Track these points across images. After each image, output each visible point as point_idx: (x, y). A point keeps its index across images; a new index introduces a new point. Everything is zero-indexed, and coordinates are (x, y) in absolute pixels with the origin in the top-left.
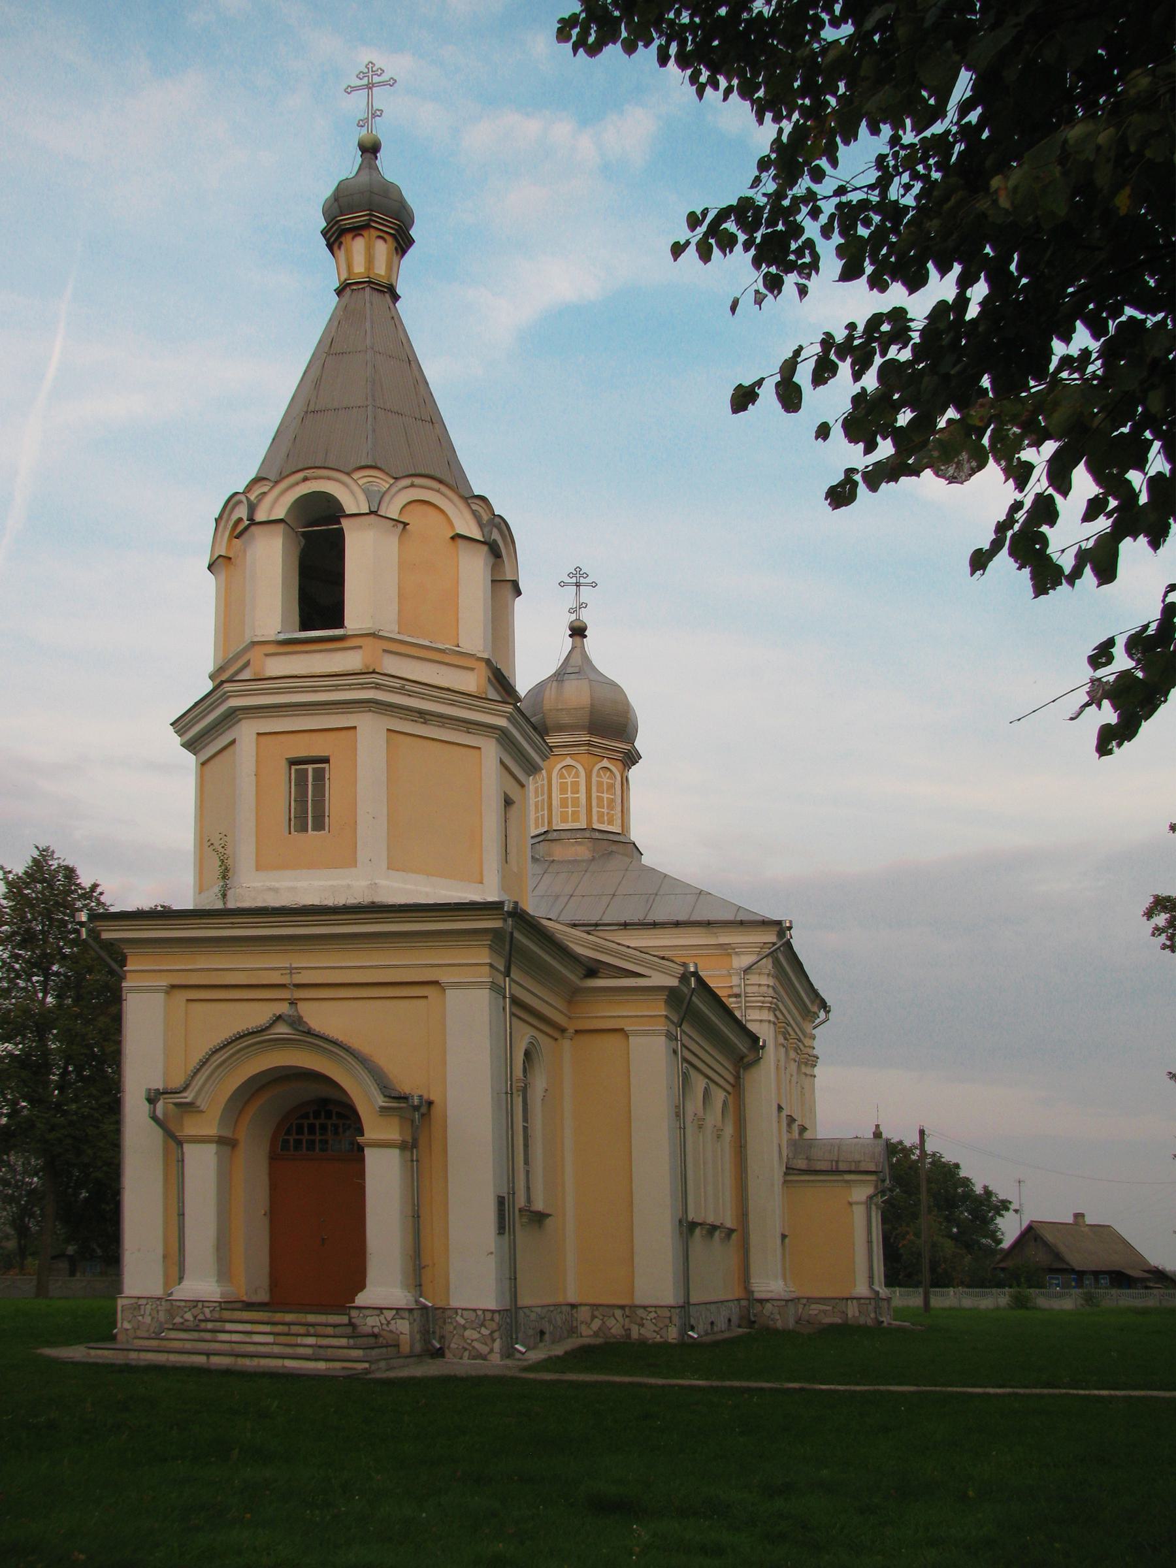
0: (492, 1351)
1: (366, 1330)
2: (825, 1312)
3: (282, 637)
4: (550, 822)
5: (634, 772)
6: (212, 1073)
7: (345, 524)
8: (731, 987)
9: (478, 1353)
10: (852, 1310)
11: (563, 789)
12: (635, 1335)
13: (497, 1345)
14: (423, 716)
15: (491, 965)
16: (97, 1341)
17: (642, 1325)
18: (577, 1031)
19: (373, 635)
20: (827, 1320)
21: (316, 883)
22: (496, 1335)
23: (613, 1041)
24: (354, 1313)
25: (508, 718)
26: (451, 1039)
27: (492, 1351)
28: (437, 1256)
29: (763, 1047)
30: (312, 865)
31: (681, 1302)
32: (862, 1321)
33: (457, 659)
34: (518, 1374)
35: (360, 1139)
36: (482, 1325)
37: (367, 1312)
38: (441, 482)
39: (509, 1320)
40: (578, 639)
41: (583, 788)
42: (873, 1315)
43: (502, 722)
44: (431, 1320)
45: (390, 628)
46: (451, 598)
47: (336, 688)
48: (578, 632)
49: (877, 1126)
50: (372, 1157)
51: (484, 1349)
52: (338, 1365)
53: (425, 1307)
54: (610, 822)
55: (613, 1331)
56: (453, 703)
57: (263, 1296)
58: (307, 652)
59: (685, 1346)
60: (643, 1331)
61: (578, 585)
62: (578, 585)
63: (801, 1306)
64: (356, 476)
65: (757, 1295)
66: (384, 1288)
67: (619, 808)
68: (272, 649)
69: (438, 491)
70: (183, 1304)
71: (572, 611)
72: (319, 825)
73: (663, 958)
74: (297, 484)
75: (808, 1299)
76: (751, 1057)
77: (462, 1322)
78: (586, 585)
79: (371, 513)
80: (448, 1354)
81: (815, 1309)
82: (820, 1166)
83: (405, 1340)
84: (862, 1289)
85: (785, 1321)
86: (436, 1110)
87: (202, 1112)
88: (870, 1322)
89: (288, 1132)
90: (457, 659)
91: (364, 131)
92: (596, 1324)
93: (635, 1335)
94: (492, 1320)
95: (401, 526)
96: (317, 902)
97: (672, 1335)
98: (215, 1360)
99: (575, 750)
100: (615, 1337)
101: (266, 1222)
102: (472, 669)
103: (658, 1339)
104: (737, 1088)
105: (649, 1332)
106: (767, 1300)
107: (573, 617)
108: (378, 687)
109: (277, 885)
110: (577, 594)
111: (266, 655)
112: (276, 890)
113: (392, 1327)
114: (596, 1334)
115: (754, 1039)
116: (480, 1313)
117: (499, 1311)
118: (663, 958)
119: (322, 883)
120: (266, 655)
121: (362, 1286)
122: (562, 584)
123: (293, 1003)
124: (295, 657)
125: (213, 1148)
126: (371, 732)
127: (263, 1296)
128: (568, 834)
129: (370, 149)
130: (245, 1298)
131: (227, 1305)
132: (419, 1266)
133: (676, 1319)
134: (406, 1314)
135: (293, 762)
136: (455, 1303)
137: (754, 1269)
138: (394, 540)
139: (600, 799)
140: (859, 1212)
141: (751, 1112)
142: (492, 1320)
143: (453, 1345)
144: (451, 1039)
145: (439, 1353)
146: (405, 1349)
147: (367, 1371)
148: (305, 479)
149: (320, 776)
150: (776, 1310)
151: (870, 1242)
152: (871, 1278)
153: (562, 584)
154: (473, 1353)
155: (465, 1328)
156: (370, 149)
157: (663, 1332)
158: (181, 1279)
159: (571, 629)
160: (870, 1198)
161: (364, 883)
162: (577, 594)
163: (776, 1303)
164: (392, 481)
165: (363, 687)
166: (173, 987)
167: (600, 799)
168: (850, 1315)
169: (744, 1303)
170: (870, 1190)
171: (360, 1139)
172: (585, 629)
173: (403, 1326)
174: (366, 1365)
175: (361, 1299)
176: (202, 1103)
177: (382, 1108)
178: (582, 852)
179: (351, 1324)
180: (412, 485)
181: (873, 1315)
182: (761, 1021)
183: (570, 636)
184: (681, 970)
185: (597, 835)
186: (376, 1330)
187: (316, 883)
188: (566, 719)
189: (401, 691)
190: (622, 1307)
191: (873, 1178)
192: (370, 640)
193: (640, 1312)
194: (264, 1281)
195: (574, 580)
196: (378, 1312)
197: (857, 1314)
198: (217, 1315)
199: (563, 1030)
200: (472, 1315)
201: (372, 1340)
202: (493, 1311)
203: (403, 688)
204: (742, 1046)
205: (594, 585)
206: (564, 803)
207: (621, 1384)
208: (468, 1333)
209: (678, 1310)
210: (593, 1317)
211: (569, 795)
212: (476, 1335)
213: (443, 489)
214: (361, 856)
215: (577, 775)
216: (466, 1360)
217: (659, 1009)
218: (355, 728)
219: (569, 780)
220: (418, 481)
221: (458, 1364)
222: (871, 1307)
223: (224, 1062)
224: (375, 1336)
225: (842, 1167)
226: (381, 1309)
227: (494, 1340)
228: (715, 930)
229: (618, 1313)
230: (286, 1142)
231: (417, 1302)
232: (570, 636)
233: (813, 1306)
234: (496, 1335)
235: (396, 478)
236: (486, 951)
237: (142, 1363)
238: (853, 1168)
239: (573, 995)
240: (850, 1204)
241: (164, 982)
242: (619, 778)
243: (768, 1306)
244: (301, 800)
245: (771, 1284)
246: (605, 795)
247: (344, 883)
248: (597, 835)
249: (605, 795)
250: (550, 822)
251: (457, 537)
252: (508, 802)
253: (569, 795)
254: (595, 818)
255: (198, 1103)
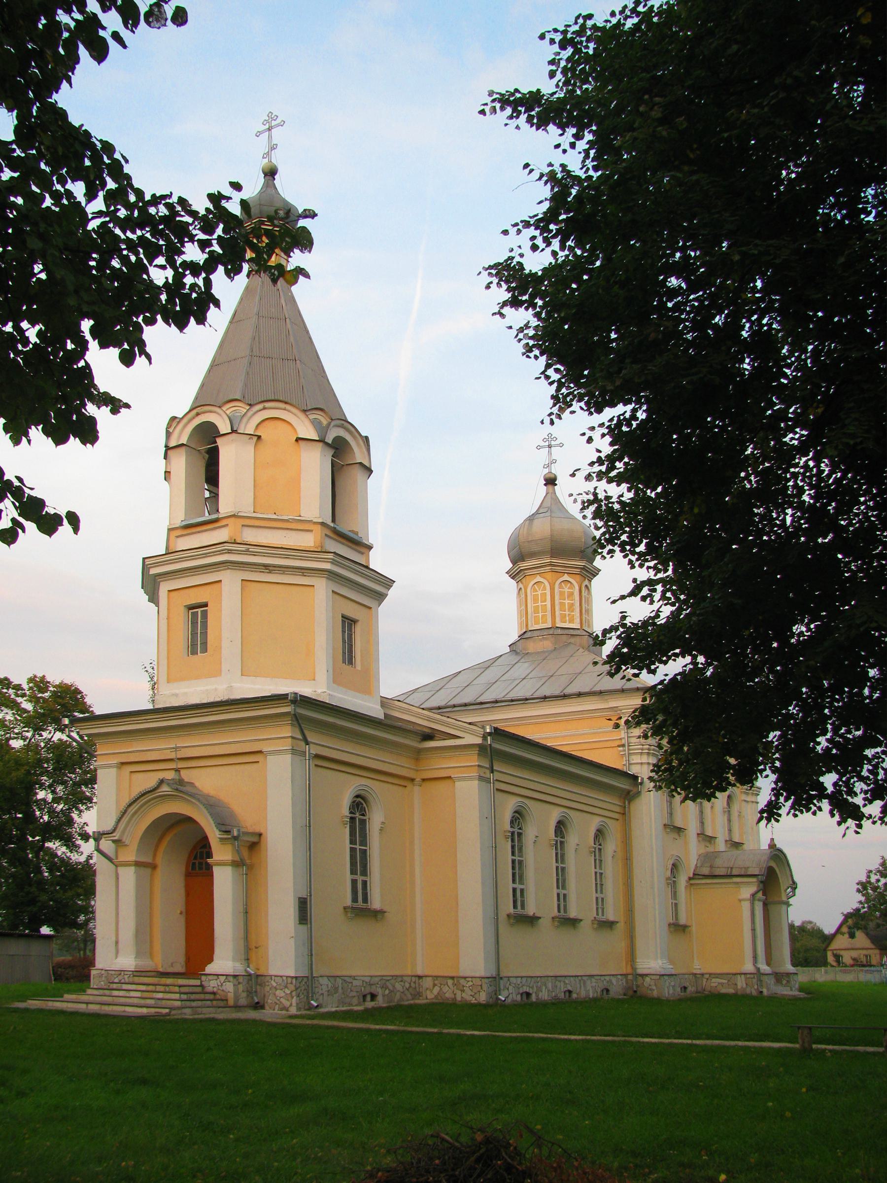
0: (291, 1005)
1: (210, 989)
2: (722, 984)
3: (184, 523)
4: (527, 626)
5: (595, 581)
6: (130, 819)
7: (219, 441)
8: (621, 739)
9: (282, 1005)
10: (741, 983)
11: (535, 600)
12: (459, 998)
13: (294, 1001)
14: (267, 568)
15: (293, 738)
16: (49, 996)
17: (463, 991)
18: (424, 780)
19: (234, 516)
20: (723, 991)
21: (198, 689)
22: (294, 993)
23: (441, 786)
24: (203, 978)
25: (332, 563)
26: (269, 791)
27: (291, 1005)
28: (269, 941)
29: (641, 783)
30: (197, 677)
31: (493, 972)
32: (748, 991)
33: (300, 525)
34: (288, 1021)
35: (209, 860)
36: (286, 987)
37: (210, 977)
38: (286, 403)
39: (305, 984)
40: (550, 487)
41: (548, 598)
42: (756, 987)
43: (327, 566)
44: (254, 982)
45: (247, 509)
46: (295, 483)
47: (206, 556)
48: (551, 481)
49: (772, 839)
50: (216, 870)
51: (287, 1004)
52: (153, 1010)
53: (250, 975)
54: (571, 621)
55: (447, 995)
56: (287, 557)
57: (179, 968)
58: (199, 532)
59: (494, 1005)
60: (464, 995)
61: (550, 446)
62: (550, 446)
63: (705, 980)
64: (224, 408)
65: (640, 971)
66: (224, 962)
67: (578, 610)
68: (179, 532)
69: (285, 409)
70: (389, 978)
71: (548, 466)
72: (205, 650)
73: (470, 724)
74: (194, 418)
75: (710, 974)
76: (635, 790)
77: (275, 984)
78: (556, 446)
79: (234, 431)
80: (267, 1007)
81: (715, 982)
82: (718, 872)
83: (231, 996)
84: (749, 967)
85: (669, 990)
86: (263, 838)
87: (126, 845)
88: (754, 993)
89: (195, 858)
90: (300, 525)
91: (266, 160)
92: (436, 990)
93: (459, 998)
94: (291, 983)
95: (255, 438)
96: (198, 702)
97: (483, 997)
98: (91, 1007)
99: (542, 570)
100: (448, 999)
101: (182, 919)
102: (311, 531)
103: (474, 1001)
104: (624, 814)
105: (467, 996)
106: (647, 975)
107: (546, 471)
108: (230, 552)
109: (177, 691)
110: (550, 453)
111: (177, 537)
112: (177, 695)
113: (224, 988)
114: (436, 997)
115: (635, 777)
116: (339, 981)
117: (296, 977)
118: (470, 724)
119: (202, 688)
120: (177, 537)
121: (210, 960)
122: (539, 447)
123: (177, 770)
124: (192, 536)
125: (133, 868)
126: (231, 581)
127: (179, 968)
128: (538, 633)
129: (271, 173)
130: (161, 970)
131: (138, 973)
132: (249, 946)
133: (485, 987)
134: (231, 979)
135: (191, 608)
136: (272, 971)
137: (639, 953)
138: (251, 448)
139: (562, 605)
140: (746, 906)
141: (636, 833)
142: (291, 983)
143: (269, 1001)
144: (269, 791)
145: (258, 1006)
146: (231, 1002)
147: (168, 1014)
148: (198, 414)
149: (205, 615)
150: (653, 983)
151: (753, 930)
152: (755, 958)
153: (539, 447)
154: (281, 1006)
155: (276, 989)
156: (271, 173)
157: (477, 996)
158: (116, 957)
159: (545, 480)
160: (753, 895)
161: (225, 686)
162: (550, 453)
163: (653, 977)
164: (248, 407)
165: (221, 553)
166: (123, 763)
167: (562, 605)
168: (739, 987)
169: (630, 977)
170: (753, 889)
171: (209, 860)
172: (555, 479)
173: (229, 987)
174: (167, 1010)
175: (210, 968)
176: (126, 840)
177: (221, 839)
178: (548, 644)
179: (202, 986)
180: (264, 408)
181: (756, 987)
182: (642, 763)
183: (545, 485)
184: (481, 731)
185: (559, 631)
186: (215, 989)
187: (198, 689)
188: (535, 548)
189: (247, 552)
190: (452, 978)
191: (754, 880)
192: (232, 520)
193: (462, 981)
194: (182, 959)
195: (547, 443)
196: (216, 977)
197: (744, 985)
198: (131, 980)
199: (413, 780)
200: (279, 980)
201: (212, 997)
202: (292, 977)
203: (248, 550)
204: (623, 784)
205: (561, 445)
206: (536, 610)
207: (350, 1029)
208: (278, 992)
209: (486, 980)
210: (435, 985)
211: (540, 603)
212: (283, 994)
213: (288, 407)
214: (224, 667)
215: (544, 589)
216: (276, 1011)
217: (473, 760)
218: (221, 581)
219: (539, 593)
220: (267, 405)
221: (269, 1014)
222: (755, 980)
223: (136, 813)
224: (214, 993)
225: (735, 872)
226: (218, 975)
227: (292, 997)
228: (606, 697)
229: (450, 982)
230: (194, 864)
231: (246, 970)
232: (545, 485)
233: (714, 980)
234: (294, 993)
235: (250, 405)
236: (289, 728)
237: (102, 1012)
238: (743, 873)
239: (418, 755)
240: (740, 901)
241: (115, 761)
242: (577, 588)
243: (648, 979)
244: (194, 634)
245: (652, 962)
246: (567, 602)
247: (214, 687)
248: (559, 631)
249: (567, 602)
250: (527, 626)
251: (298, 440)
252: (348, 623)
253: (540, 603)
254: (558, 619)
255: (124, 840)
